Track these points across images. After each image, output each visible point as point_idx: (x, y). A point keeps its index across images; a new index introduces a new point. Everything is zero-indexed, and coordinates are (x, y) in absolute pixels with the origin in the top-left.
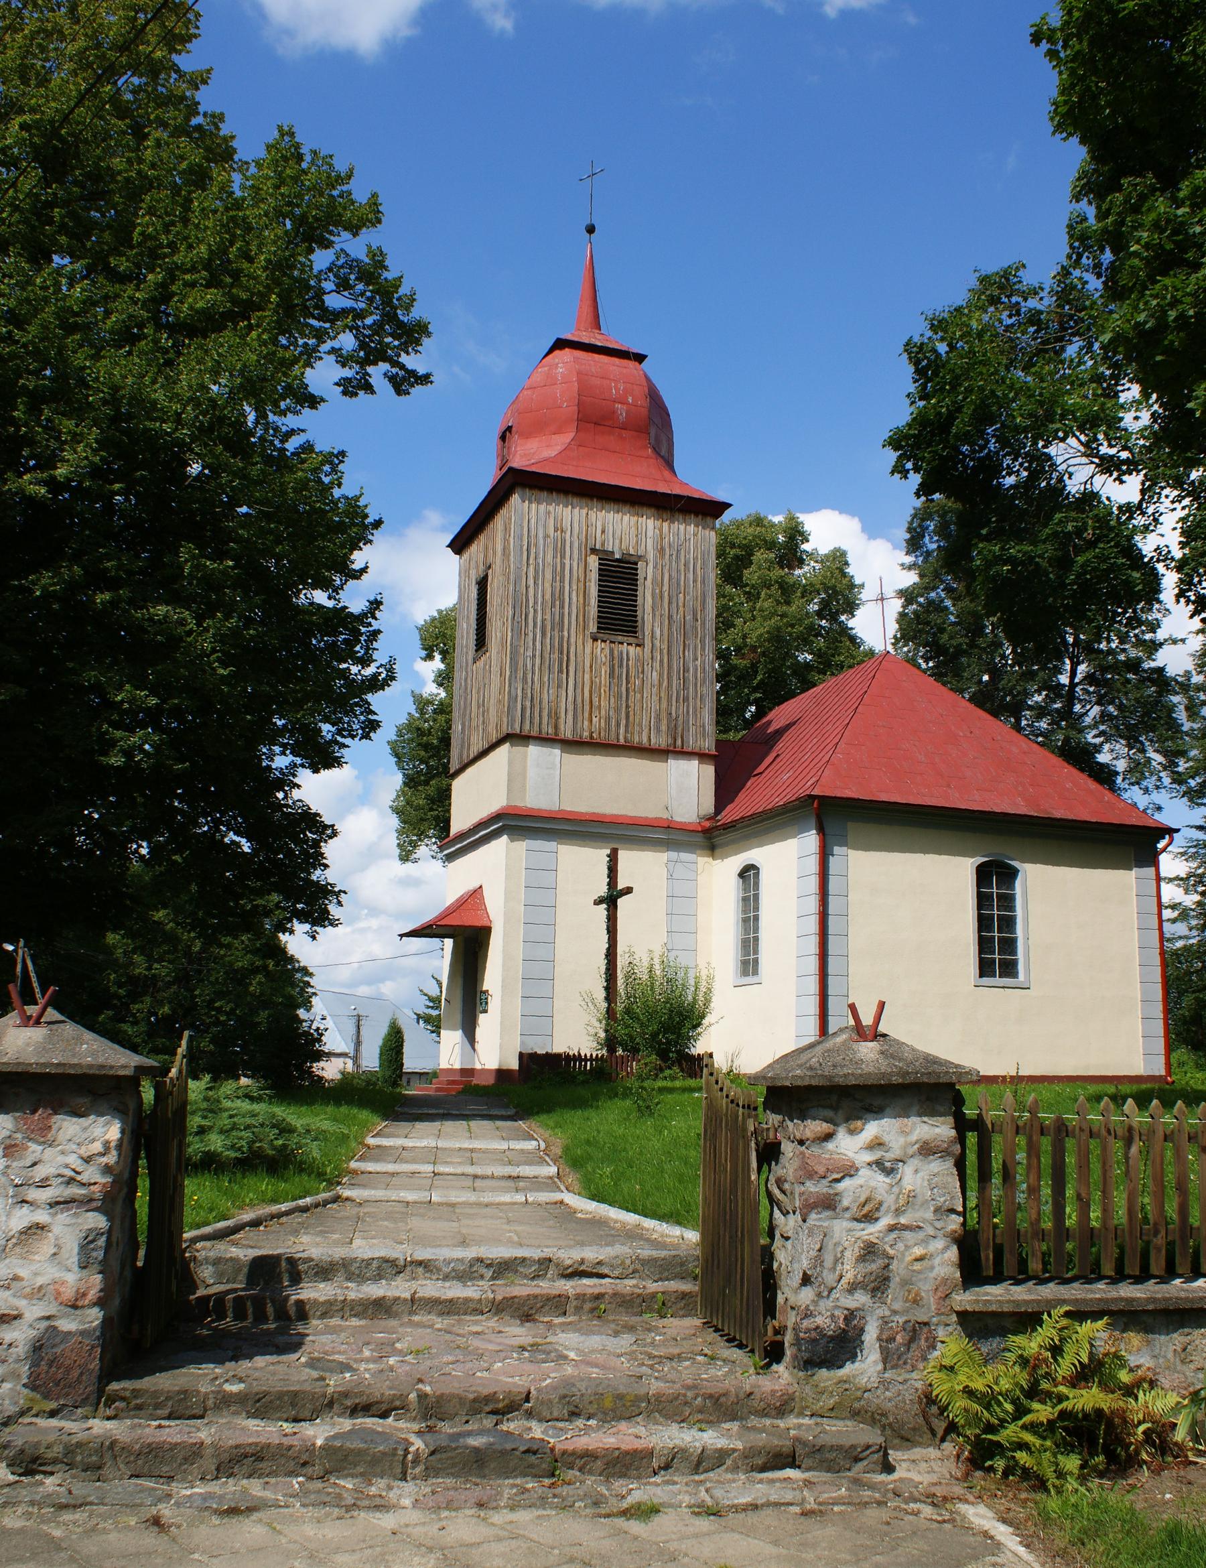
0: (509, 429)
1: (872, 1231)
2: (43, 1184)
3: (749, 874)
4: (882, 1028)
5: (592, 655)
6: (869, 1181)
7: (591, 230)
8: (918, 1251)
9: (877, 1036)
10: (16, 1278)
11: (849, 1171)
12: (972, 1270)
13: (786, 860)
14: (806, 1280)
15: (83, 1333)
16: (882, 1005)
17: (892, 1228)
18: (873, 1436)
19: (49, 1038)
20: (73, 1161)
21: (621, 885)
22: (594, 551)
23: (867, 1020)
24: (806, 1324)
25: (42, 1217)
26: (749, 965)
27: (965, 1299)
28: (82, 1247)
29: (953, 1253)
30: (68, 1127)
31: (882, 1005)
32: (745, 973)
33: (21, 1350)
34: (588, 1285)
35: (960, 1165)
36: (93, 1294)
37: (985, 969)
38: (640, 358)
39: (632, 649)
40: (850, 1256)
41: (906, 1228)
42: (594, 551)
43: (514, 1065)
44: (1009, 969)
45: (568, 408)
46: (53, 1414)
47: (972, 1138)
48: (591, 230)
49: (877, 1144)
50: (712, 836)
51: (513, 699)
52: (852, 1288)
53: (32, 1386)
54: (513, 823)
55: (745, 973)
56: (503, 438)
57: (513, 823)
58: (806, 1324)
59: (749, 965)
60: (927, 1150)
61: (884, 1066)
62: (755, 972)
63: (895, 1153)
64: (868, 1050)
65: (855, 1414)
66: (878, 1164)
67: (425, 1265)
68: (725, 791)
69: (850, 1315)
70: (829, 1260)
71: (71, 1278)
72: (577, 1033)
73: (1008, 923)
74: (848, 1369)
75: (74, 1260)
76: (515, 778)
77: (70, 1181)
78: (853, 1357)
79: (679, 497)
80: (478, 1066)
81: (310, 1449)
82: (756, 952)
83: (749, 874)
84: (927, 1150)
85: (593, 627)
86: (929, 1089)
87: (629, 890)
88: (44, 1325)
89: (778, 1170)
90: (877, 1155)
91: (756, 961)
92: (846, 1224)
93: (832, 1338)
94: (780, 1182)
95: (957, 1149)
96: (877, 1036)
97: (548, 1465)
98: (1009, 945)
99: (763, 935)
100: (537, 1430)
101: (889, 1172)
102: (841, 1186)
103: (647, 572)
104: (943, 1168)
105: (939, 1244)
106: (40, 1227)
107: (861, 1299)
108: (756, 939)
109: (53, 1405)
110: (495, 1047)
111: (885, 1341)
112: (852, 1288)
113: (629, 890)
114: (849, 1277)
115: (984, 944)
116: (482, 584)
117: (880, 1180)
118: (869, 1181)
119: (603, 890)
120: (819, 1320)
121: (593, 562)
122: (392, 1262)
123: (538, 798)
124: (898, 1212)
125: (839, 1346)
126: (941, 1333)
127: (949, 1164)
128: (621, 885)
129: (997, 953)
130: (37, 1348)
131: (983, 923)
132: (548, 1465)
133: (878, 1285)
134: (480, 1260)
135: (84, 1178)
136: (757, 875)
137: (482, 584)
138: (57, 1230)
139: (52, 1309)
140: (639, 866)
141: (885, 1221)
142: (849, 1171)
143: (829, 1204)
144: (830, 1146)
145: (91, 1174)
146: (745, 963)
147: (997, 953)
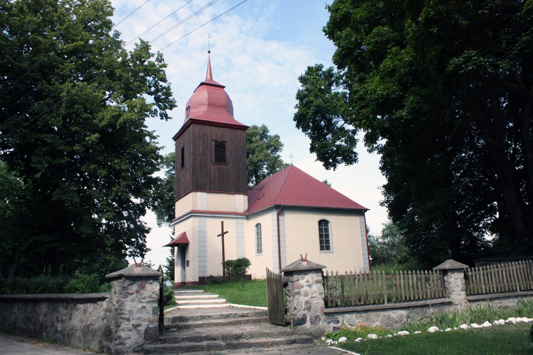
0: (189, 107)
1: (307, 298)
2: (144, 298)
3: (258, 225)
4: (307, 259)
5: (213, 168)
6: (306, 288)
7: (209, 52)
8: (316, 302)
9: (306, 261)
10: (140, 317)
11: (302, 287)
12: (327, 306)
13: (268, 220)
14: (295, 309)
15: (154, 327)
16: (307, 254)
17: (311, 297)
18: (310, 337)
19: (143, 269)
20: (150, 293)
21: (225, 231)
22: (213, 140)
23: (304, 258)
24: (296, 317)
25: (144, 305)
26: (259, 250)
27: (326, 310)
28: (153, 311)
29: (323, 302)
30: (148, 286)
31: (307, 254)
32: (258, 252)
33: (143, 331)
34: (245, 318)
35: (323, 285)
36: (156, 320)
37: (322, 248)
38: (224, 87)
39: (224, 166)
40: (303, 303)
41: (314, 297)
42: (213, 140)
43: (197, 280)
44: (328, 248)
45: (206, 102)
46: (149, 344)
47: (325, 280)
48: (209, 52)
49: (307, 281)
50: (248, 215)
51: (193, 181)
52: (304, 309)
53: (145, 338)
54: (193, 214)
55: (258, 252)
56: (187, 109)
57: (193, 214)
58: (296, 317)
59: (259, 250)
60: (317, 282)
61: (308, 266)
62: (261, 252)
63: (311, 283)
64: (305, 263)
65: (306, 334)
66: (308, 285)
67: (209, 317)
68: (251, 203)
69: (304, 315)
70: (299, 304)
71: (151, 317)
72: (217, 271)
73: (327, 236)
74: (304, 325)
75: (151, 313)
76: (194, 202)
77: (150, 297)
78: (305, 323)
79: (236, 125)
80: (187, 281)
81: (203, 346)
82: (261, 246)
83: (258, 225)
84: (317, 282)
85: (214, 161)
86: (318, 270)
87: (227, 232)
88: (146, 326)
89: (288, 288)
90: (307, 284)
91: (261, 249)
92: (303, 297)
93: (301, 320)
94: (288, 291)
95: (323, 281)
96: (306, 261)
97: (249, 346)
98: (328, 242)
99: (263, 242)
100: (246, 341)
101: (310, 287)
102: (301, 290)
103: (227, 145)
104: (320, 285)
105: (320, 300)
106: (144, 307)
107: (306, 312)
108: (261, 243)
109: (149, 342)
110: (192, 276)
111: (311, 319)
112: (304, 309)
113: (227, 232)
114: (303, 308)
115: (321, 242)
116: (183, 149)
117: (308, 288)
118: (306, 288)
119: (220, 233)
120: (298, 316)
121: (213, 143)
122: (203, 316)
123: (200, 207)
124: (312, 294)
125: (303, 321)
126: (321, 317)
127: (321, 284)
128: (225, 231)
129: (325, 244)
130: (146, 331)
131: (321, 236)
132: (249, 346)
133: (309, 309)
134: (222, 315)
135: (153, 296)
136: (260, 226)
137: (183, 149)
138: (101, 323)
139: (148, 323)
140: (230, 224)
141: (310, 296)
142: (302, 287)
143: (299, 293)
144: (298, 282)
145: (154, 296)
146: (258, 250)
147: (325, 244)
